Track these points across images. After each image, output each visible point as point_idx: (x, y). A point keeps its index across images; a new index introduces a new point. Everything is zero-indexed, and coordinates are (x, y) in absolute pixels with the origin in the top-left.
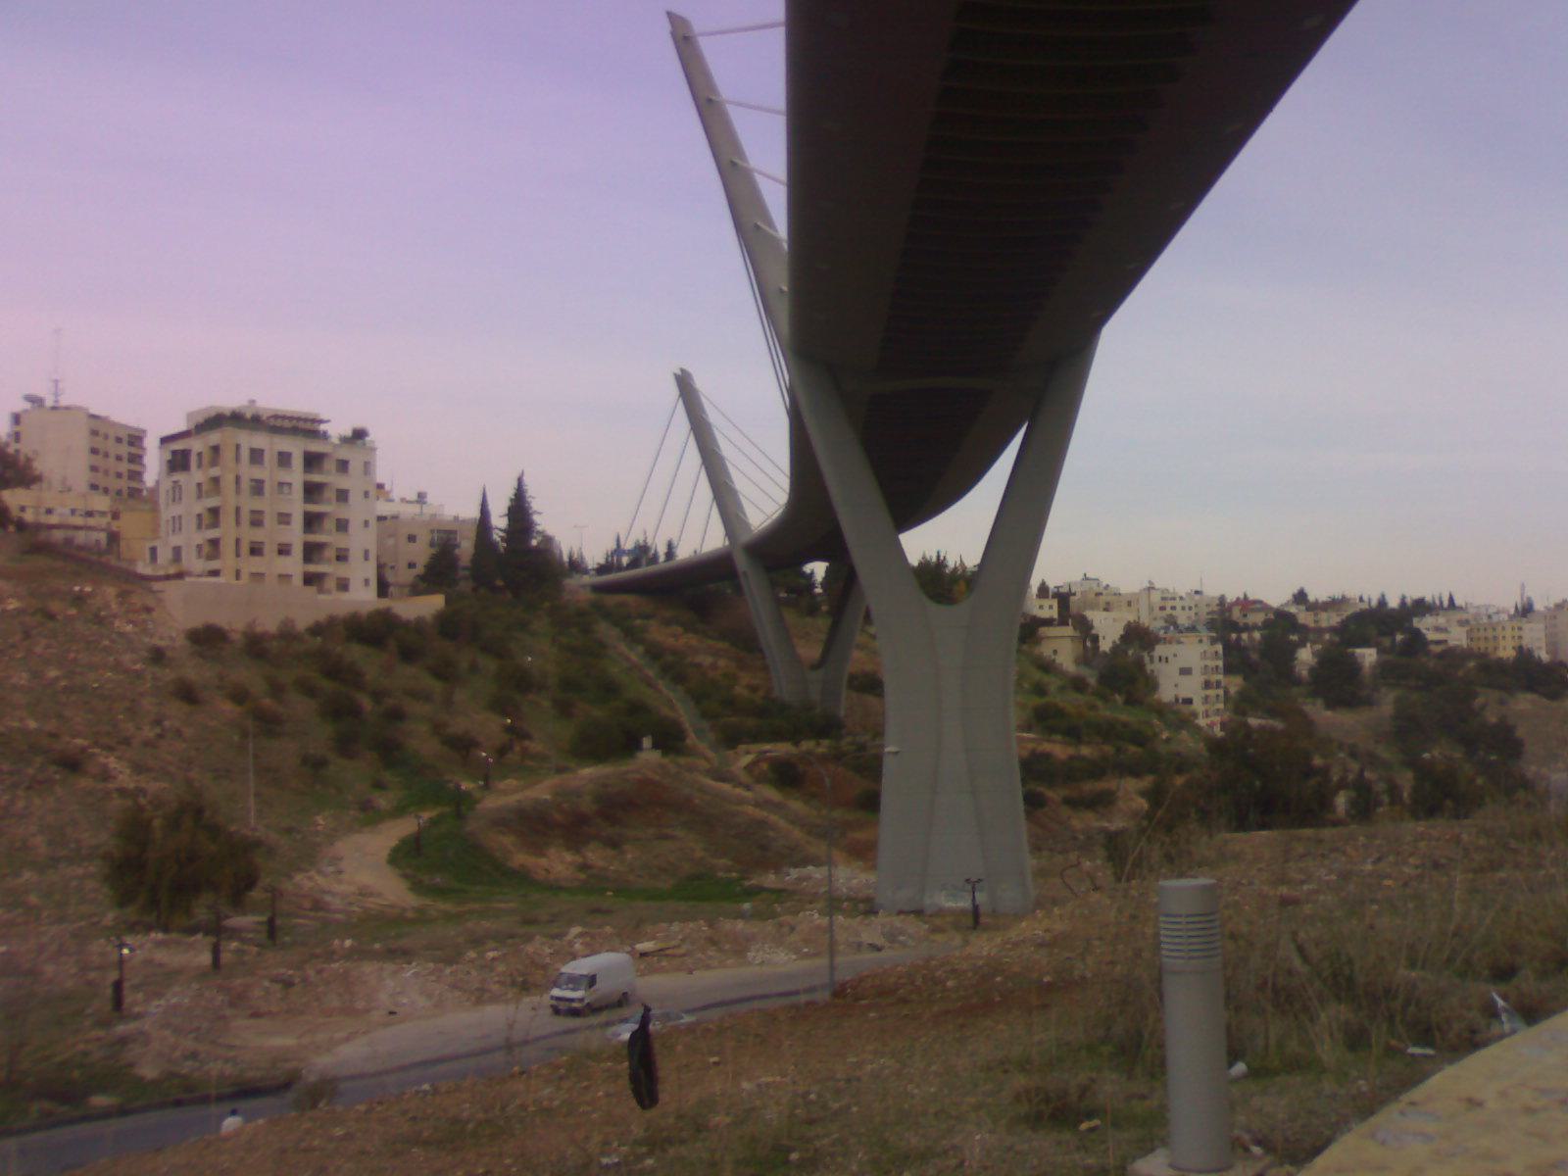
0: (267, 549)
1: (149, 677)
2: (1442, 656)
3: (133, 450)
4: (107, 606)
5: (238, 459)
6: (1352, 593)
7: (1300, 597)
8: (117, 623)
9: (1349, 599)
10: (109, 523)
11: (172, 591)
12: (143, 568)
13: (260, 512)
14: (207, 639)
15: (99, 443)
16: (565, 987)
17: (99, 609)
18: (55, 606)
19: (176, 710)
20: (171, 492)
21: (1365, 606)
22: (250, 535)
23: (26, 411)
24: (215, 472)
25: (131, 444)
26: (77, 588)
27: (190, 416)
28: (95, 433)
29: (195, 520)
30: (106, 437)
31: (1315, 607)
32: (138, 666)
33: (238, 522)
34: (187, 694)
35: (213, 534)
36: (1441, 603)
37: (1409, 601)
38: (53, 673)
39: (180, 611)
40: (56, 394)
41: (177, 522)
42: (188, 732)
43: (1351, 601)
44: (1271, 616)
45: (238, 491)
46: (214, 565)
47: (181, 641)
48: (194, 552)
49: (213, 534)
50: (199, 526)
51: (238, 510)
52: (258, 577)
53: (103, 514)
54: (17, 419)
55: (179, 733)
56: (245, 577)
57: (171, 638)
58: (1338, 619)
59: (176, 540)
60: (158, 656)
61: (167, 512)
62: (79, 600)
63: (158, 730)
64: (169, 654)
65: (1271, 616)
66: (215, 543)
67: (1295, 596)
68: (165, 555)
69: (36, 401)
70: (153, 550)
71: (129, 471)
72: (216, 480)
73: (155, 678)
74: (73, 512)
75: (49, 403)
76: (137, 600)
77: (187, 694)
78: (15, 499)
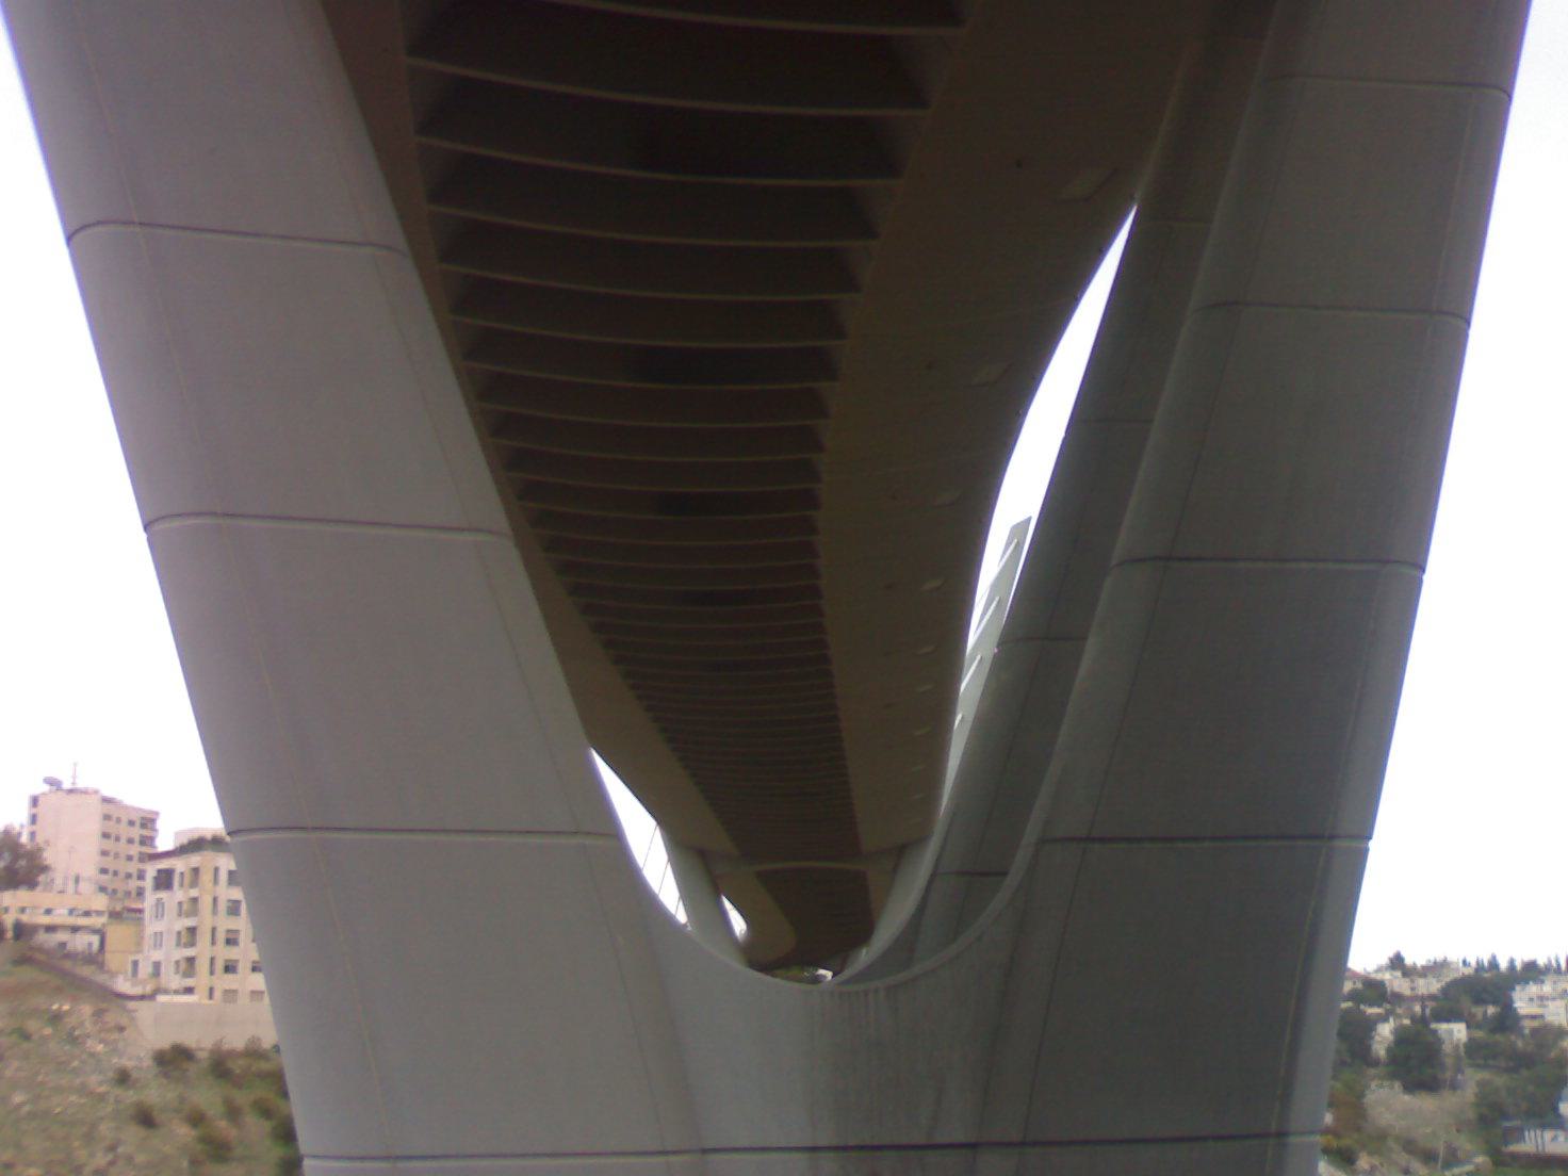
0: (240, 967)
1: (112, 1100)
2: (1535, 1031)
3: (145, 832)
4: (82, 1024)
5: (216, 880)
6: (1455, 955)
7: (1397, 962)
8: (89, 1043)
9: (1451, 963)
10: (104, 925)
11: (144, 1011)
12: (123, 985)
13: (237, 932)
14: (174, 1059)
15: (112, 827)
16: (1481, 1062)
17: (74, 1029)
18: (32, 1025)
19: (133, 1134)
20: (154, 909)
21: (1468, 971)
22: (224, 953)
23: (44, 794)
24: (194, 893)
25: (143, 826)
26: (55, 1007)
27: (177, 835)
28: (107, 817)
29: (174, 937)
30: (119, 820)
31: (1408, 972)
32: (103, 1089)
33: (213, 942)
34: (146, 1118)
35: (190, 952)
36: (1559, 965)
37: (1518, 965)
38: (18, 1098)
39: (151, 1030)
40: (74, 777)
41: (159, 937)
42: (140, 1158)
43: (1452, 967)
44: (1359, 986)
45: (215, 911)
46: (189, 982)
47: (148, 1062)
48: (172, 969)
49: (190, 952)
50: (178, 944)
51: (214, 930)
52: (230, 994)
53: (99, 913)
54: (35, 801)
55: (130, 1159)
56: (218, 994)
57: (139, 1059)
58: (1439, 986)
59: (157, 955)
60: (123, 1078)
61: (152, 927)
62: (56, 1018)
63: (110, 1157)
64: (135, 1075)
65: (1359, 986)
66: (191, 961)
67: (1391, 960)
68: (145, 970)
69: (53, 783)
70: (135, 964)
71: (140, 853)
72: (195, 900)
73: (117, 1102)
74: (71, 912)
75: (67, 785)
76: (111, 1018)
77: (146, 1118)
78: (14, 904)
